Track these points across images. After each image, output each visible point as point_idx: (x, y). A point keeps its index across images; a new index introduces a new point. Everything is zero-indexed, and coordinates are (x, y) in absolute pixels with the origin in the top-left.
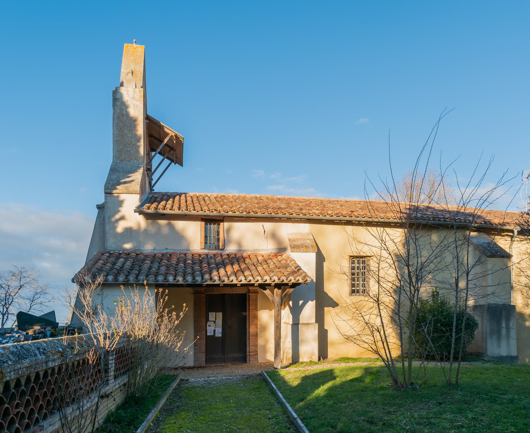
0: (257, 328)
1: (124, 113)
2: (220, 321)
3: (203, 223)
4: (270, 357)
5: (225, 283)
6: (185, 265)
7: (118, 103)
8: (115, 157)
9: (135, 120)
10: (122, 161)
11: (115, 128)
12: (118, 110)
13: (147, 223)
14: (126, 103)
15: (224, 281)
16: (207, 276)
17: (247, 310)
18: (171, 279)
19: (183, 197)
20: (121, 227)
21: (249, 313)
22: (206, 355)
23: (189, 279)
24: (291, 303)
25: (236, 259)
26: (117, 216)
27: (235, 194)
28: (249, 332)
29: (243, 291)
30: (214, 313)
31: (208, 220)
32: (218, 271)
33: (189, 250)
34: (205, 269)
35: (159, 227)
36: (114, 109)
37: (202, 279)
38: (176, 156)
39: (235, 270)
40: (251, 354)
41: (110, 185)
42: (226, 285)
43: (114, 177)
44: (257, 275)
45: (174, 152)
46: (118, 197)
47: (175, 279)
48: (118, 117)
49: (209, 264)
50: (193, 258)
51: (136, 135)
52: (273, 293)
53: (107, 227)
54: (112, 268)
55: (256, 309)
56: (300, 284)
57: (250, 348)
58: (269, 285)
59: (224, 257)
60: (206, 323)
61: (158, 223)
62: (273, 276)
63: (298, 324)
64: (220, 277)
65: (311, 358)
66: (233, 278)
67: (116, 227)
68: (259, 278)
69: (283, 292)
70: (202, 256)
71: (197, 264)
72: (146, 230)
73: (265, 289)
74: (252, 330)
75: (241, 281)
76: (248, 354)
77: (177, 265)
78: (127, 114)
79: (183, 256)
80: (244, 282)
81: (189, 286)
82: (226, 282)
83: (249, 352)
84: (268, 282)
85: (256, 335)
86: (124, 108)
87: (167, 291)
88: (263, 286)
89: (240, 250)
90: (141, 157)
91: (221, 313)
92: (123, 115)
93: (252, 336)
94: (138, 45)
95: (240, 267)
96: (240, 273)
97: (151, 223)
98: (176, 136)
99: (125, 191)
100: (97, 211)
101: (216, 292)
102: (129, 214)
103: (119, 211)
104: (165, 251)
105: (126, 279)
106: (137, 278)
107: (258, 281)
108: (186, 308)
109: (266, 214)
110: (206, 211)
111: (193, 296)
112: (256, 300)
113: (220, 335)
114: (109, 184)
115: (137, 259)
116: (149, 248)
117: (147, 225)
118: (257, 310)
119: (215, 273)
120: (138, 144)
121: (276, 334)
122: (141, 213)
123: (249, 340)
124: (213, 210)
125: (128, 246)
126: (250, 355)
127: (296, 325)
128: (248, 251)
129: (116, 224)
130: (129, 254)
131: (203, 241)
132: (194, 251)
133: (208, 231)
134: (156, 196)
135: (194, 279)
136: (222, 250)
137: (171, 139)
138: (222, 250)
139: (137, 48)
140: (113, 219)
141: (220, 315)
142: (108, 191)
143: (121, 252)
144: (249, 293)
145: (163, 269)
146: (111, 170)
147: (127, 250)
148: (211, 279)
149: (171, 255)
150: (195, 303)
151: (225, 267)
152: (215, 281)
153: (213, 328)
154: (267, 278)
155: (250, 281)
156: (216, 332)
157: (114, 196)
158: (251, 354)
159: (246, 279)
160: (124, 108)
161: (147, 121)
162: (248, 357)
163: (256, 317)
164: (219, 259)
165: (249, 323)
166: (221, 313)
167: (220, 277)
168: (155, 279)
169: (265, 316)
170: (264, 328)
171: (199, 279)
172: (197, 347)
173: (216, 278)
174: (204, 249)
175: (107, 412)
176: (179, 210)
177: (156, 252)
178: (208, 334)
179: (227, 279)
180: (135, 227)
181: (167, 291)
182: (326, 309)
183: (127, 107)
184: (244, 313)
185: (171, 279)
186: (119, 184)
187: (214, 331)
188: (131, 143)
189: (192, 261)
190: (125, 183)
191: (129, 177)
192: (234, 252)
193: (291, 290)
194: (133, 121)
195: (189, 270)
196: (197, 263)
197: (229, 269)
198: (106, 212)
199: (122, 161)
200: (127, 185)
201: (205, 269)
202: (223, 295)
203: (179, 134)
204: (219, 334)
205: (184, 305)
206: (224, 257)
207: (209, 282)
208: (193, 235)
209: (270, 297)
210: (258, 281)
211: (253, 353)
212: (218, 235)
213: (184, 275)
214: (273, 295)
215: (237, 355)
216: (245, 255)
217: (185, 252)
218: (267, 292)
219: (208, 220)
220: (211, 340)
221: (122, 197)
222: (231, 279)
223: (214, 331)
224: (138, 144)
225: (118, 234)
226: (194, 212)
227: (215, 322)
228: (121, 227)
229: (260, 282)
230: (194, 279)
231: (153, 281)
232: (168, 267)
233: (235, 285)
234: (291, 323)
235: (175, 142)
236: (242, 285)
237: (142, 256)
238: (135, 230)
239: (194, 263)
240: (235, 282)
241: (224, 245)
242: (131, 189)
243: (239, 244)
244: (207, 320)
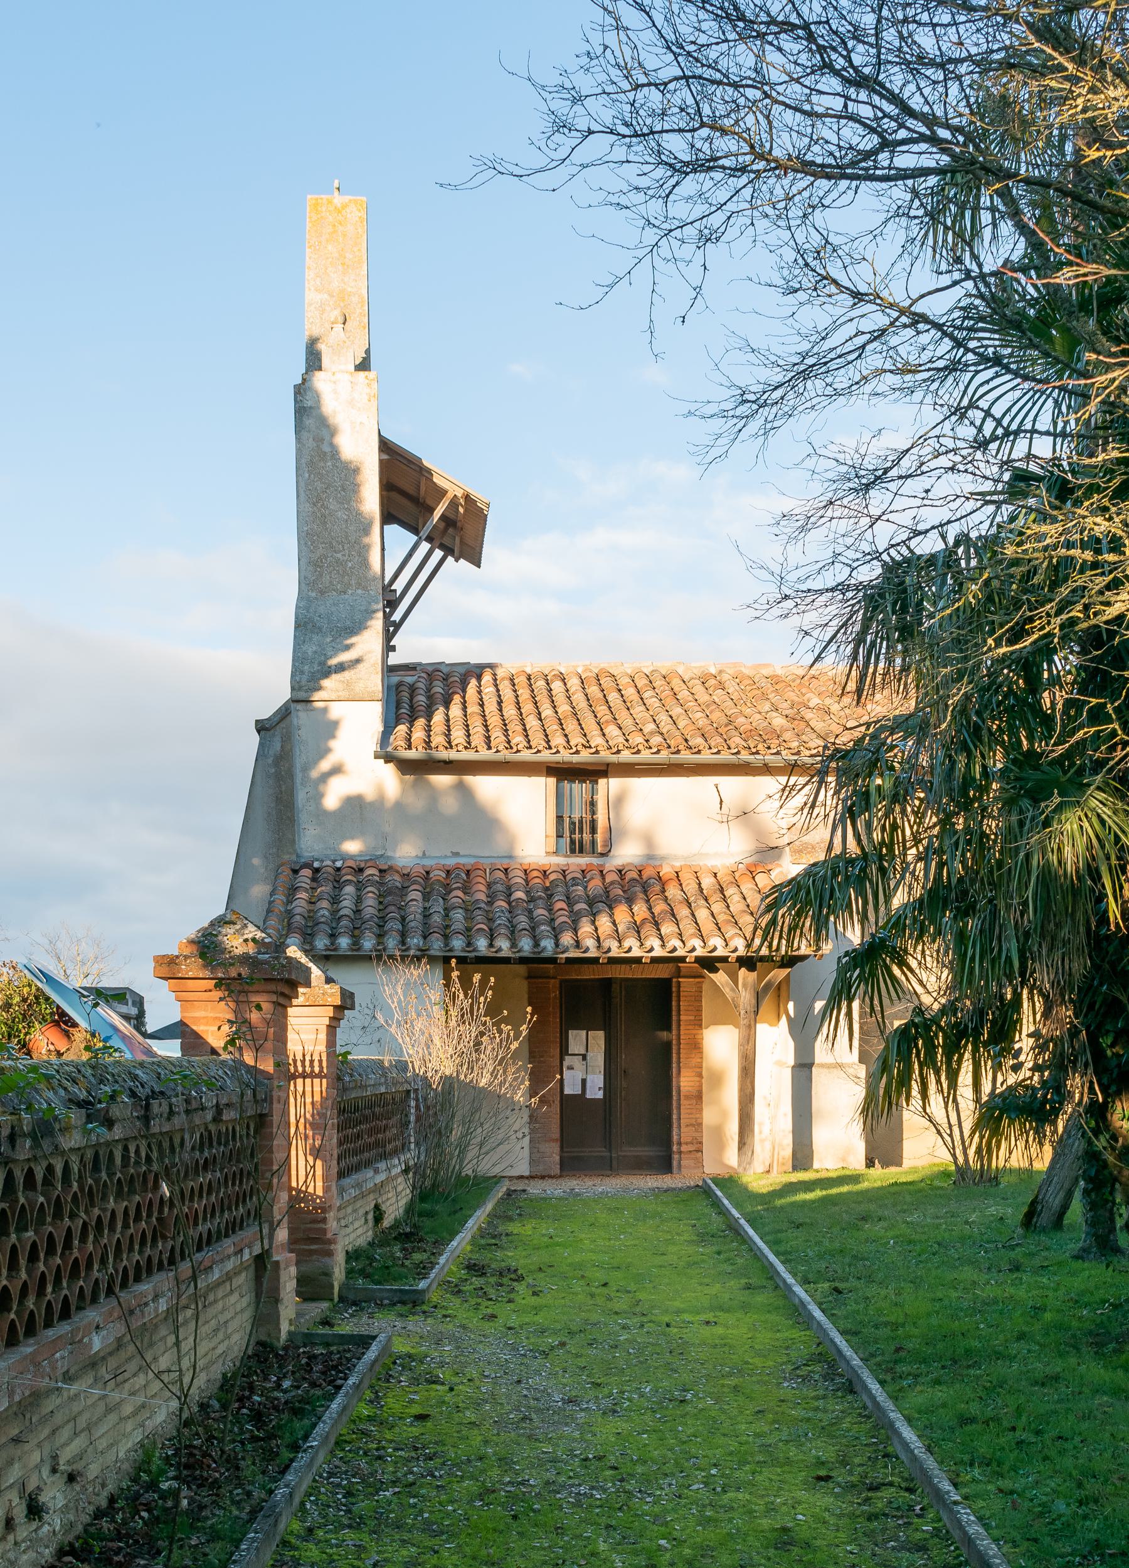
0: (700, 1075)
1: (326, 448)
2: (598, 1057)
3: (552, 781)
4: (732, 1157)
5: (611, 954)
6: (509, 903)
7: (309, 422)
8: (305, 582)
9: (356, 471)
10: (322, 593)
11: (302, 495)
12: (311, 443)
13: (402, 781)
14: (331, 421)
15: (609, 950)
16: (567, 939)
17: (674, 1026)
18: (482, 944)
19: (487, 678)
20: (333, 796)
22: (562, 1147)
23: (526, 945)
24: (791, 1006)
25: (642, 885)
26: (325, 765)
28: (679, 1087)
29: (662, 972)
31: (564, 773)
32: (593, 922)
33: (510, 857)
34: (562, 918)
35: (434, 794)
36: (298, 439)
37: (557, 945)
38: (461, 541)
39: (638, 919)
40: (684, 1148)
41: (305, 678)
42: (613, 961)
43: (310, 649)
44: (693, 936)
45: (459, 532)
46: (325, 710)
47: (491, 945)
48: (311, 463)
49: (570, 901)
50: (527, 882)
51: (359, 514)
52: (736, 983)
53: (301, 796)
54: (310, 902)
55: (698, 1024)
56: (803, 958)
57: (682, 1132)
58: (724, 959)
59: (608, 879)
60: (562, 1060)
61: (428, 783)
62: (732, 937)
63: (810, 1065)
64: (598, 939)
65: (844, 1160)
66: (631, 942)
67: (320, 796)
68: (697, 943)
69: (760, 979)
70: (552, 877)
71: (540, 902)
72: (399, 805)
73: (715, 970)
74: (685, 1082)
75: (652, 950)
76: (675, 1148)
77: (490, 903)
78: (335, 453)
79: (502, 876)
80: (658, 952)
81: (523, 961)
82: (615, 952)
83: (679, 1144)
84: (720, 952)
85: (699, 1097)
86: (324, 432)
87: (492, 979)
88: (710, 963)
89: (650, 857)
90: (374, 579)
91: (601, 1034)
92: (323, 456)
93: (687, 1097)
94: (347, 198)
95: (650, 909)
96: (649, 929)
97: (415, 785)
98: (467, 497)
99: (344, 694)
100: (256, 738)
101: (588, 974)
102: (355, 761)
103: (328, 750)
104: (451, 862)
105: (379, 944)
106: (403, 943)
107: (693, 950)
108: (532, 1015)
109: (726, 757)
110: (561, 749)
111: (524, 985)
113: (600, 1095)
114: (302, 673)
115: (388, 885)
116: (407, 853)
117: (403, 791)
118: (700, 1026)
119: (586, 928)
120: (366, 540)
121: (742, 1090)
122: (388, 758)
123: (679, 1108)
124: (580, 748)
125: (352, 847)
126: (680, 1153)
127: (804, 1067)
128: (676, 858)
129: (321, 788)
130: (361, 870)
131: (552, 831)
132: (526, 861)
133: (566, 803)
134: (409, 680)
135: (536, 944)
136: (602, 855)
137: (454, 503)
138: (602, 855)
139: (345, 206)
140: (314, 774)
141: (598, 1038)
142: (302, 695)
143: (339, 864)
144: (679, 976)
145: (458, 915)
146: (298, 626)
147: (352, 857)
148: (578, 944)
149: (468, 873)
151: (611, 908)
152: (587, 950)
153: (579, 1075)
154: (716, 941)
155: (674, 949)
156: (588, 1084)
157: (314, 709)
158: (684, 1148)
159: (663, 946)
160: (327, 438)
161: (385, 457)
162: (676, 1157)
163: (697, 1046)
164: (595, 885)
165: (679, 1062)
166: (601, 1034)
167: (598, 939)
168: (446, 945)
169: (719, 1044)
170: (717, 1079)
171: (548, 944)
173: (590, 943)
174: (556, 853)
175: (138, 1436)
176: (489, 748)
177: (428, 863)
179: (616, 944)
180: (370, 794)
181: (492, 979)
183: (332, 431)
184: (664, 1035)
185: (482, 944)
186: (327, 672)
187: (584, 1081)
188: (347, 537)
189: (527, 893)
190: (341, 668)
191: (348, 648)
192: (636, 861)
193: (784, 972)
194: (350, 473)
195: (522, 921)
196: (540, 898)
197: (622, 914)
198: (284, 744)
199: (322, 593)
200: (346, 675)
201: (562, 918)
202: (607, 983)
203: (475, 493)
204: (595, 1092)
205: (529, 1009)
206: (608, 879)
207: (572, 954)
208: (523, 816)
209: (727, 991)
210: (693, 950)
211: (691, 1148)
212: (593, 813)
213: (513, 932)
214: (736, 985)
215: (646, 1152)
216: (666, 871)
217: (505, 863)
218: (720, 978)
219: (564, 773)
220: (573, 1107)
221: (336, 711)
222: (626, 944)
223: (584, 1081)
224: (366, 540)
225: (326, 813)
226: (526, 755)
227: (584, 1057)
228: (333, 796)
229: (700, 952)
230: (536, 944)
231: (441, 950)
232: (469, 910)
233: (638, 960)
234: (792, 1062)
235: (461, 510)
236: (655, 960)
237: (397, 877)
238: (371, 804)
239: (532, 900)
240: (636, 952)
241: (609, 843)
242: (359, 687)
243: (649, 841)
244: (564, 1051)
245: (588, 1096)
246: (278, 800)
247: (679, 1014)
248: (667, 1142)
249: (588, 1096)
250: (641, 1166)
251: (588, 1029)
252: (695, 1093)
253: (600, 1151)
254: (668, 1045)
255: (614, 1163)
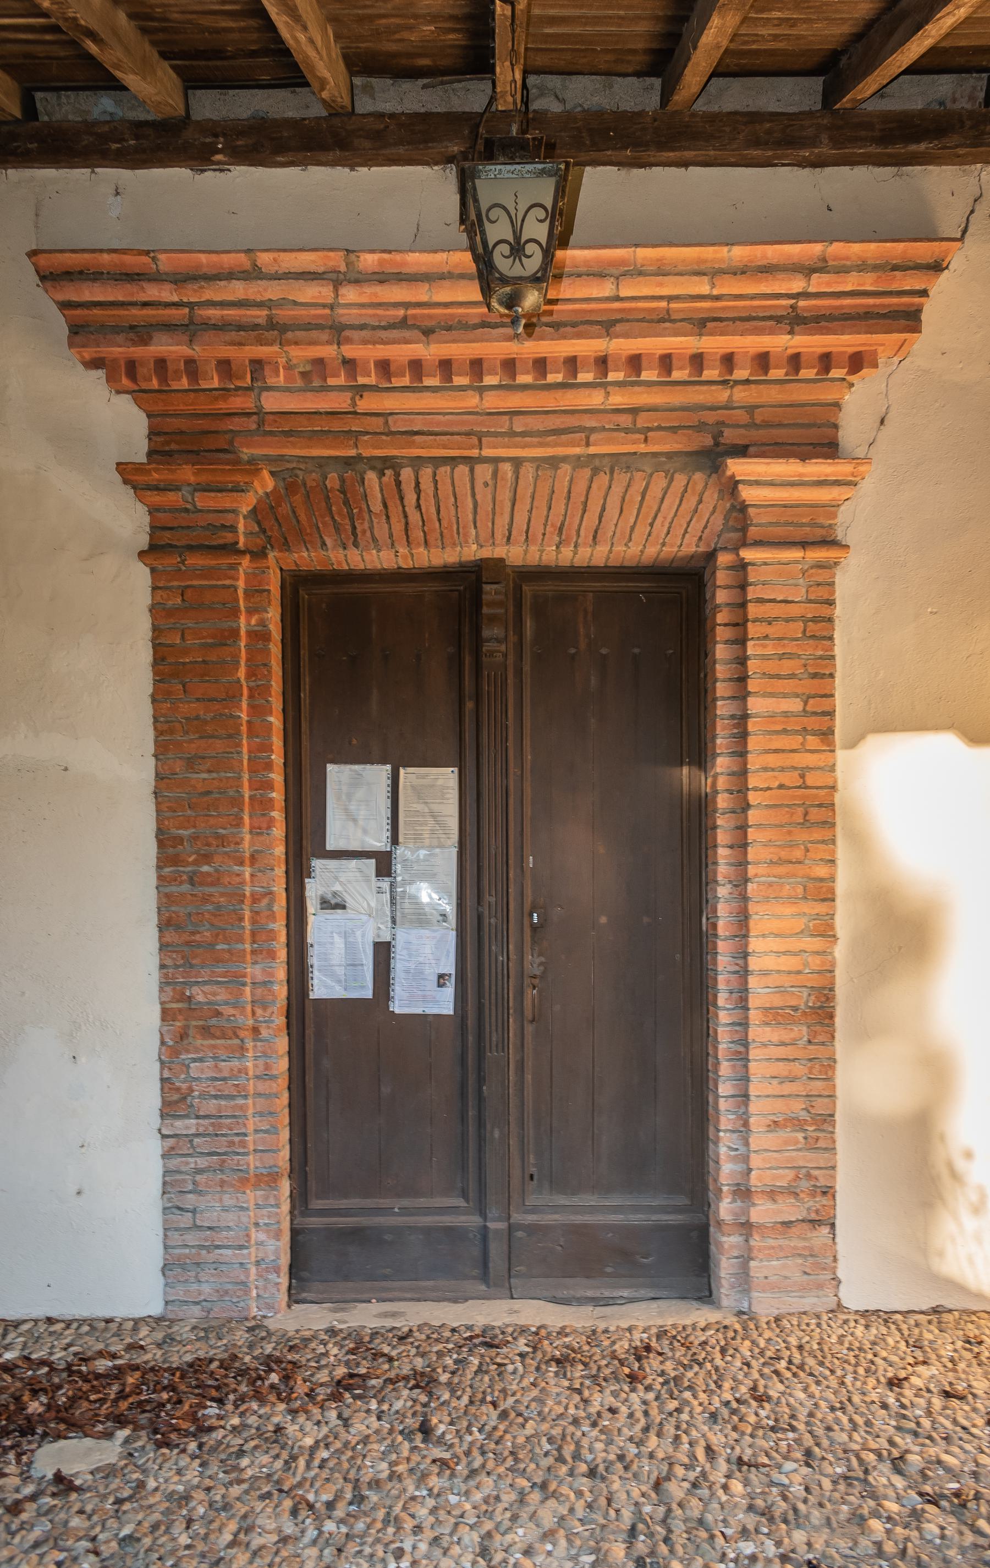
17: (722, 739)
21: (742, 773)
22: (300, 1200)
27: (548, 1322)
30: (380, 774)
57: (749, 1148)
60: (298, 873)
74: (764, 947)
76: (726, 1208)
83: (743, 1192)
91: (445, 779)
111: (141, 576)
112: (819, 625)
123: (742, 1059)
126: (746, 1227)
150: (160, 657)
156: (399, 966)
158: (762, 1212)
163: (817, 811)
166: (445, 779)
172: (187, 1126)
178: (323, 987)
182: (452, 1013)
187: (383, 952)
204: (426, 984)
211: (789, 1210)
220: (337, 1048)
223: (383, 952)
227: (384, 864)
244: (305, 839)
245: (398, 1007)
246: (68, 273)
247: (742, 696)
248: (686, 1167)
249: (398, 1007)
250: (589, 1262)
251: (399, 757)
252: (803, 999)
253: (450, 1211)
254: (694, 820)
255: (496, 1250)
